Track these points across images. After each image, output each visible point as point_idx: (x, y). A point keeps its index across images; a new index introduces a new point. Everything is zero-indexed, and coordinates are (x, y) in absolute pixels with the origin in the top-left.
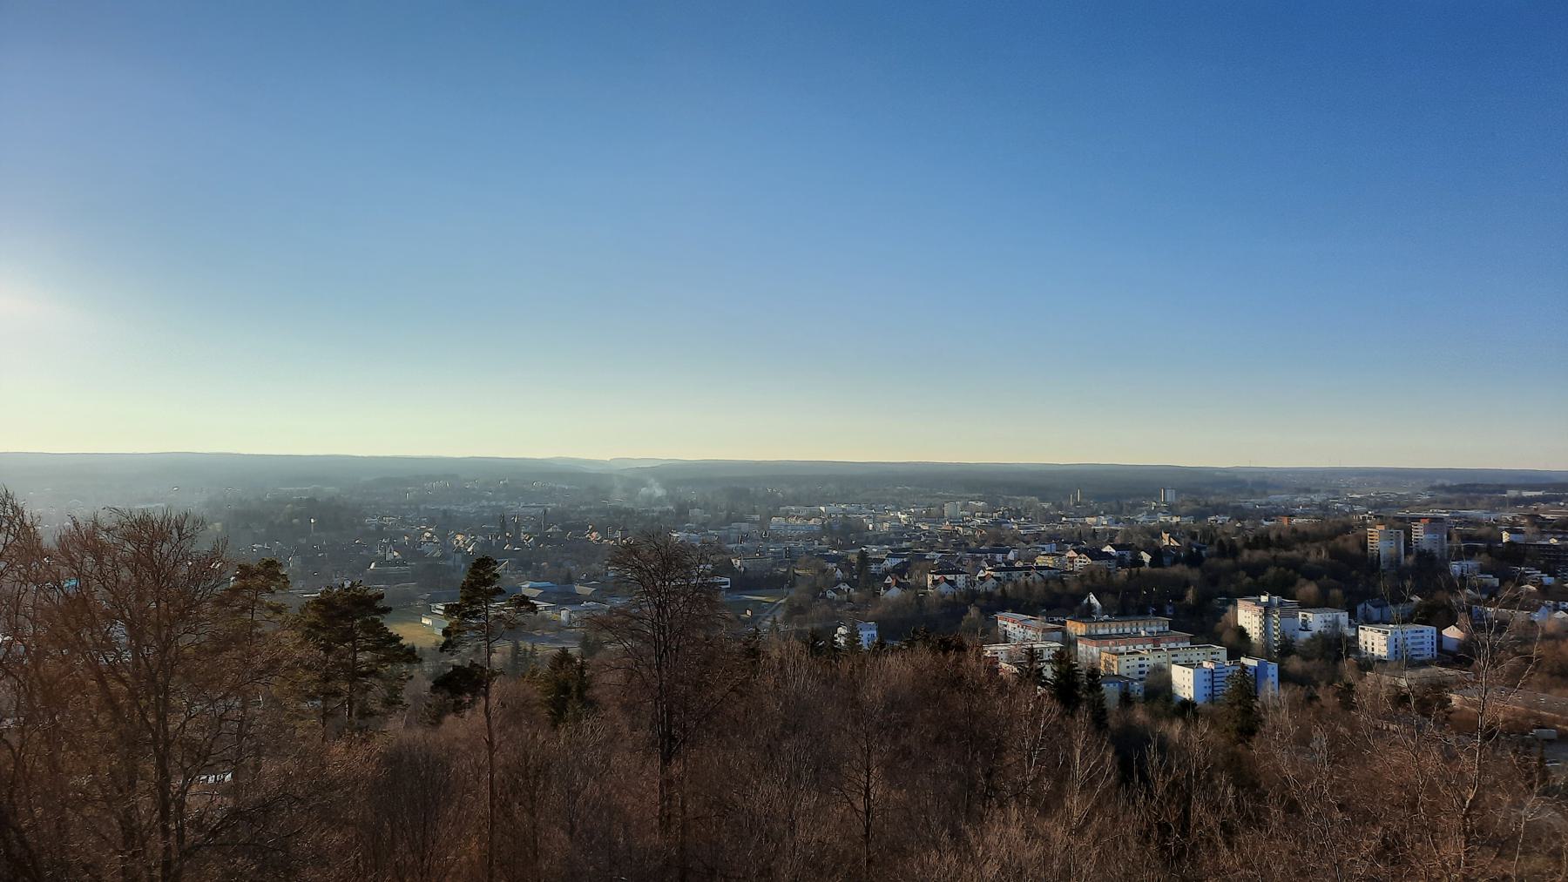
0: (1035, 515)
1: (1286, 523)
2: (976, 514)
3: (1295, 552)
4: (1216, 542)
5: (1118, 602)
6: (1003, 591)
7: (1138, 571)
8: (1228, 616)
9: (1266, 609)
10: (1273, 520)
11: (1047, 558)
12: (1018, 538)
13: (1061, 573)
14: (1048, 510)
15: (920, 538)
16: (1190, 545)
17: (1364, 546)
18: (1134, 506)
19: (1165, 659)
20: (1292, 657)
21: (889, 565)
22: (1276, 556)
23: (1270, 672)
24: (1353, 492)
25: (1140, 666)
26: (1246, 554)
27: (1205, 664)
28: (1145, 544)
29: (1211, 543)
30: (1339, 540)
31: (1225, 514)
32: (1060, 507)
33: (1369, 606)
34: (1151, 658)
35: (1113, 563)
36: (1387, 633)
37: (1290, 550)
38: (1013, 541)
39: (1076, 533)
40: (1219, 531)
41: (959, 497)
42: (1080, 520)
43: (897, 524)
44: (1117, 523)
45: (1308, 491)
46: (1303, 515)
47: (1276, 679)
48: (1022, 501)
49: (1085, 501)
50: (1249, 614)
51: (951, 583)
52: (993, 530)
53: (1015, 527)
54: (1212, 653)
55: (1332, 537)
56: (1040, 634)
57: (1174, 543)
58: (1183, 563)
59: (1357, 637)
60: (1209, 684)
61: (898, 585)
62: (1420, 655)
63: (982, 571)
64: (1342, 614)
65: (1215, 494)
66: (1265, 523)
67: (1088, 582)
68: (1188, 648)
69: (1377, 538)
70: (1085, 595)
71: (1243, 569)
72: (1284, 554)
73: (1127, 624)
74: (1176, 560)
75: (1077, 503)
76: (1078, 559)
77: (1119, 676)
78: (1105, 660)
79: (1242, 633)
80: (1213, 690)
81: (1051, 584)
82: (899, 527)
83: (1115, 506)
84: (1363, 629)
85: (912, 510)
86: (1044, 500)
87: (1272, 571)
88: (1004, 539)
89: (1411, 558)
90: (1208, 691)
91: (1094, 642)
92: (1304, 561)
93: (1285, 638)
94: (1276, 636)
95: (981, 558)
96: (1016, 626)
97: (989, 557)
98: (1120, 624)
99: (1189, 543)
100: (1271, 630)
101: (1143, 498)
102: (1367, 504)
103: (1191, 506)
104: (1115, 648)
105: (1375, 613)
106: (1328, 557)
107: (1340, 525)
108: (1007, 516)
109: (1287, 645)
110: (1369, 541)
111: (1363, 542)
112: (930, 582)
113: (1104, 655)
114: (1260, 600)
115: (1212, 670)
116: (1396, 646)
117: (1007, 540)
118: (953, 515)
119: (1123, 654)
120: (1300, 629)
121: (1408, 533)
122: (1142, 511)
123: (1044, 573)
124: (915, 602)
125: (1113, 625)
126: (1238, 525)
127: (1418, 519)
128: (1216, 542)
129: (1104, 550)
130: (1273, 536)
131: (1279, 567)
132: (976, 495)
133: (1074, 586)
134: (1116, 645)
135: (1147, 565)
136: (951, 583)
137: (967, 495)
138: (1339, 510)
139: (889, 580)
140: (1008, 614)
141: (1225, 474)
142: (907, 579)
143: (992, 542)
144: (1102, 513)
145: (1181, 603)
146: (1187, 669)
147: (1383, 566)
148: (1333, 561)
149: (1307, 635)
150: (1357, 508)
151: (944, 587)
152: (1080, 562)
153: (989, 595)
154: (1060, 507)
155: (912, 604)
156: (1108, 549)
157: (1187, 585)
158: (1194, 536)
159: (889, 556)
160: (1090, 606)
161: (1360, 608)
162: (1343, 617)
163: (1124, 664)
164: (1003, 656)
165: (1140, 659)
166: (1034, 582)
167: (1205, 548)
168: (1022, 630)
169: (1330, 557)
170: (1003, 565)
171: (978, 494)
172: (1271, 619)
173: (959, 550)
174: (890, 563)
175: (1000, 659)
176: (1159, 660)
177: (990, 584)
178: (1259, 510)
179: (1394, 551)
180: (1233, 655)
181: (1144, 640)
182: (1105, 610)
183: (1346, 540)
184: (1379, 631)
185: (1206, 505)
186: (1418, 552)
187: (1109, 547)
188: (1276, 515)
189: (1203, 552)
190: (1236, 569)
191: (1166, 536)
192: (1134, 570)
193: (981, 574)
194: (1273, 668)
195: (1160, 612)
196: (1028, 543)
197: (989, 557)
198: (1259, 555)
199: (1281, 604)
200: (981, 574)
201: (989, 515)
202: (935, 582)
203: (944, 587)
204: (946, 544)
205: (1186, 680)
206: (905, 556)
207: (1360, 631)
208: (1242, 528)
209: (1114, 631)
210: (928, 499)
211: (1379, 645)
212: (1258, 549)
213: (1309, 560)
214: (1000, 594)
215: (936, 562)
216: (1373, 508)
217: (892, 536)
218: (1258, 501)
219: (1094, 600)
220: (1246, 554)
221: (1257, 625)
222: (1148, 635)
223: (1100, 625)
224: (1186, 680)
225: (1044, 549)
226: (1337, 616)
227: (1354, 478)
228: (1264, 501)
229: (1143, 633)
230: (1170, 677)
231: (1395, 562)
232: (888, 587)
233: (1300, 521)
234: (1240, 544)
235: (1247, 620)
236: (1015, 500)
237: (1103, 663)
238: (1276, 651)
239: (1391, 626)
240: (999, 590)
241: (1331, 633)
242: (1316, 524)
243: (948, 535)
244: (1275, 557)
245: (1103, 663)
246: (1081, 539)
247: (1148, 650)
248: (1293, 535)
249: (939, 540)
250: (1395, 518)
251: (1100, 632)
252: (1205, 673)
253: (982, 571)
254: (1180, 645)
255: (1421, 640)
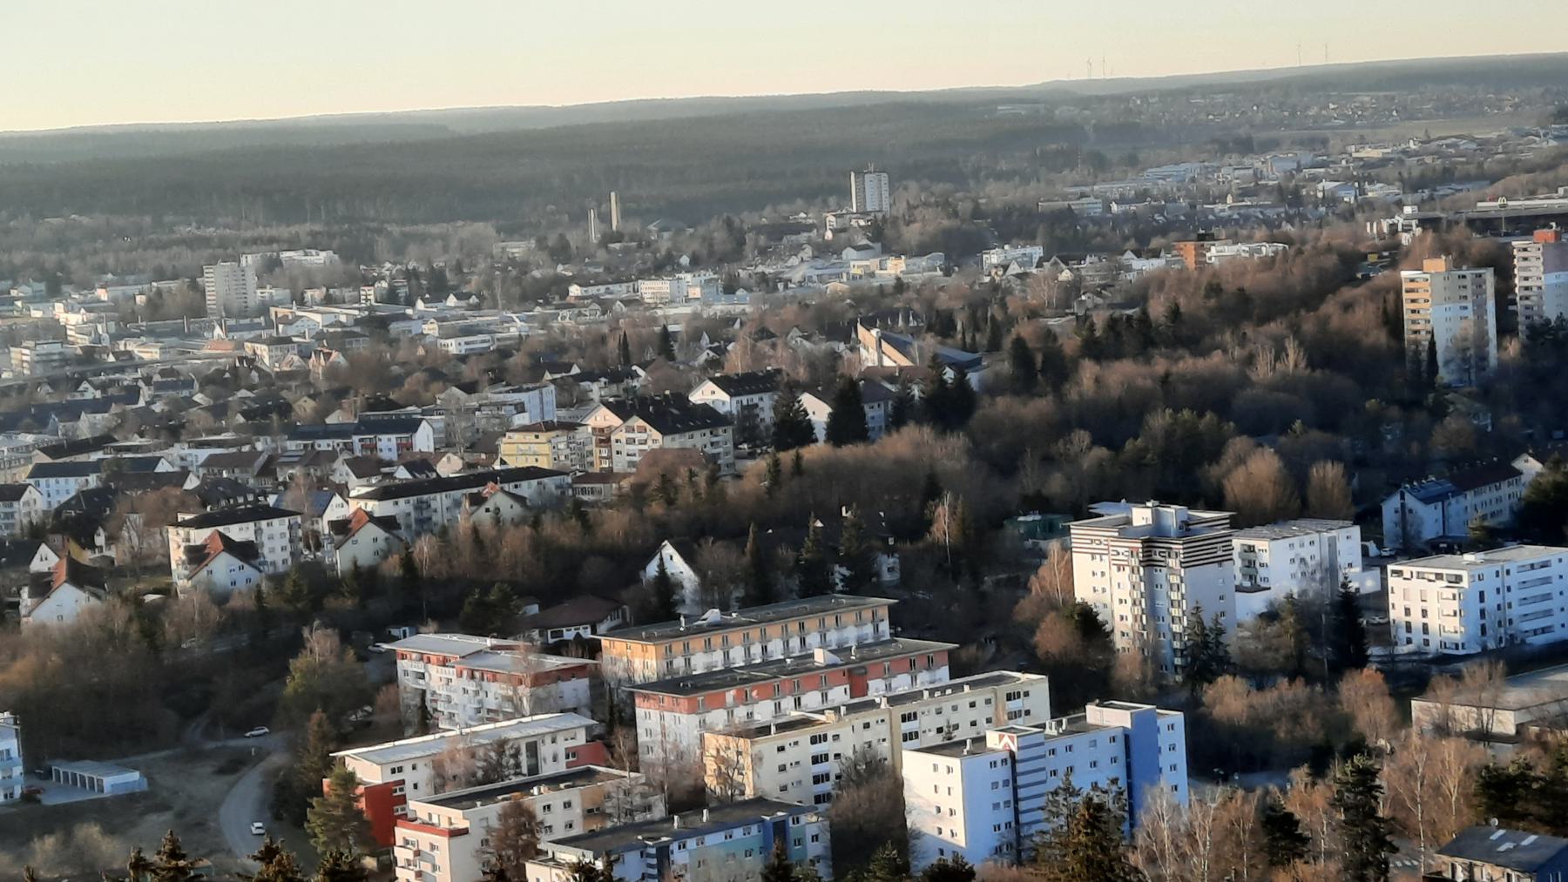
0: (489, 285)
1: (1190, 262)
2: (309, 294)
3: (1217, 358)
4: (1007, 342)
5: (747, 559)
6: (408, 563)
7: (798, 458)
8: (1046, 578)
9: (1149, 544)
10: (1155, 254)
11: (530, 437)
12: (440, 372)
13: (577, 480)
14: (524, 267)
15: (132, 393)
16: (937, 363)
17: (1393, 321)
18: (781, 231)
19: (882, 730)
20: (1220, 680)
21: (41, 505)
22: (1167, 375)
23: (1164, 740)
24: (1362, 142)
25: (816, 760)
26: (1088, 371)
27: (993, 740)
28: (812, 365)
29: (994, 346)
30: (1330, 307)
31: (1030, 238)
32: (561, 253)
33: (1411, 501)
34: (845, 732)
35: (725, 436)
36: (1458, 579)
37: (1204, 353)
38: (426, 385)
39: (613, 344)
40: (1013, 305)
41: (245, 243)
42: (621, 290)
43: (57, 348)
44: (730, 289)
45: (1246, 146)
46: (1236, 228)
47: (1180, 756)
48: (444, 238)
49: (635, 226)
50: (1103, 565)
51: (246, 552)
52: (362, 347)
53: (431, 329)
54: (1009, 697)
55: (1311, 299)
56: (524, 691)
57: (893, 359)
58: (919, 422)
59: (1383, 593)
60: (1005, 794)
61: (80, 576)
62: (1544, 630)
63: (337, 499)
64: (1343, 533)
65: (1000, 176)
66: (1139, 264)
67: (656, 508)
68: (943, 690)
69: (1427, 296)
70: (653, 550)
71: (1083, 425)
72: (1188, 364)
73: (774, 630)
74: (901, 413)
75: (609, 238)
76: (623, 436)
77: (760, 802)
78: (720, 760)
79: (1089, 623)
80: (1017, 812)
81: (550, 526)
82: (65, 360)
83: (720, 236)
84: (1399, 573)
85: (102, 294)
86: (511, 231)
87: (1159, 421)
88: (398, 381)
89: (1513, 347)
90: (1006, 815)
91: (683, 701)
92: (1245, 381)
93: (1201, 623)
94: (1178, 623)
95: (332, 456)
96: (450, 673)
97: (357, 446)
98: (755, 633)
99: (935, 357)
100: (1162, 603)
101: (799, 202)
102: (1401, 180)
103: (931, 222)
104: (741, 712)
105: (1429, 519)
106: (1302, 365)
107: (1331, 261)
108: (403, 292)
109: (1206, 645)
110: (1405, 296)
111: (1391, 306)
112: (177, 555)
113: (713, 741)
114: (1129, 521)
115: (1012, 754)
116: (1482, 613)
117: (408, 384)
118: (236, 305)
119: (764, 730)
120: (1239, 589)
121: (1503, 267)
122: (797, 248)
123: (527, 488)
124: (134, 627)
125: (735, 636)
126: (1066, 275)
127: (1526, 224)
128: (1007, 342)
129: (696, 397)
130: (1157, 309)
131: (1177, 410)
132: (303, 230)
133: (615, 524)
134: (744, 699)
135: (820, 432)
136: (246, 552)
137: (273, 232)
138: (1331, 200)
139: (45, 560)
140: (430, 640)
141: (1022, 111)
142: (104, 550)
143: (365, 392)
144: (685, 260)
145: (921, 545)
146: (943, 761)
147: (1445, 375)
148: (1318, 373)
149: (1257, 603)
150: (1374, 192)
151: (223, 568)
152: (631, 441)
153: (365, 579)
154: (561, 253)
155: (125, 636)
156: (707, 394)
157: (933, 491)
158: (942, 325)
159: (40, 472)
160: (666, 583)
161: (1390, 508)
162: (1348, 541)
163: (773, 759)
164: (418, 777)
165: (814, 740)
166: (497, 520)
167: (974, 364)
168: (471, 687)
169: (1311, 364)
170: (402, 474)
171: (308, 227)
172: (1161, 575)
173: (261, 431)
174: (44, 497)
175: (408, 787)
176: (868, 736)
177: (366, 546)
178: (1118, 221)
179: (1468, 327)
180: (1066, 701)
181: (821, 679)
182: (712, 591)
183: (1348, 307)
184: (1439, 576)
185: (977, 213)
186: (1532, 328)
187: (710, 386)
188: (1163, 231)
189: (973, 378)
190: (1062, 426)
191: (868, 337)
192: (787, 457)
193: (337, 510)
194: (1172, 725)
195: (862, 584)
196: (470, 388)
197: (357, 446)
198: (1123, 374)
199: (1186, 527)
200: (337, 510)
201: (348, 293)
202: (197, 556)
203: (223, 568)
204: (219, 411)
205: (943, 790)
206: (95, 467)
207: (1393, 581)
208: (1074, 289)
209: (738, 657)
210: (151, 253)
211: (1441, 614)
212: (1118, 356)
213: (1254, 377)
214: (398, 572)
215: (192, 483)
216: (1413, 186)
217: (44, 394)
218: (1114, 189)
219: (676, 564)
220: (1088, 371)
221: (1125, 592)
222: (835, 659)
223: (697, 642)
224: (943, 790)
225: (520, 408)
226: (1332, 544)
227: (1365, 98)
228: (1129, 187)
229: (820, 657)
230: (899, 785)
231: (1471, 356)
232: (43, 586)
233: (1230, 250)
234: (1070, 344)
235: (1100, 583)
236: (422, 239)
237: (711, 766)
238: (1178, 661)
239: (1469, 557)
240: (394, 560)
241: (1317, 593)
242: (1268, 263)
243: (222, 381)
244: (1165, 379)
245: (711, 766)
246: (627, 361)
247: (836, 710)
248: (1212, 302)
249: (198, 398)
250: (1471, 223)
251: (701, 663)
252: (993, 764)
253: (337, 499)
254: (924, 678)
255: (1545, 589)
